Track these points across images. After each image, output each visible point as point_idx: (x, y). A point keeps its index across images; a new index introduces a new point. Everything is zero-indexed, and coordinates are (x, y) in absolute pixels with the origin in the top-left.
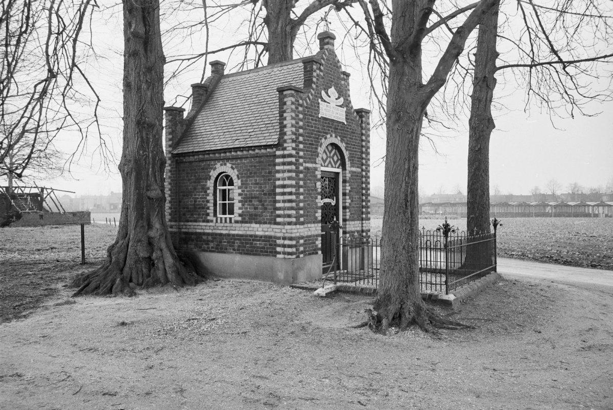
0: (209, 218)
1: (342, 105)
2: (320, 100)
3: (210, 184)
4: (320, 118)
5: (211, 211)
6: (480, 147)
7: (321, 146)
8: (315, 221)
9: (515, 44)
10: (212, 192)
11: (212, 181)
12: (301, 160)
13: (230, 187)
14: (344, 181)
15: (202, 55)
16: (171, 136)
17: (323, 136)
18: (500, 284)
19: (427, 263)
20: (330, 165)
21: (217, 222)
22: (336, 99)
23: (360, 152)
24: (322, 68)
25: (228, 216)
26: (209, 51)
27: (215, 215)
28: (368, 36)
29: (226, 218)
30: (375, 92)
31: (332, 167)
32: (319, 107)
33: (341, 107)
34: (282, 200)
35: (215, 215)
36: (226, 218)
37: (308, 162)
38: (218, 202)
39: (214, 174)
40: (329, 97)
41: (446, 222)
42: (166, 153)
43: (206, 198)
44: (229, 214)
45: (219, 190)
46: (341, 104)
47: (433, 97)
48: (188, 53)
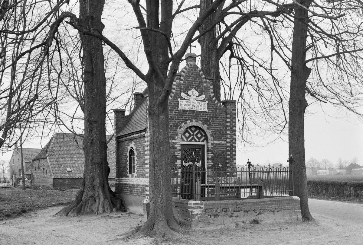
1: (204, 99)
2: (179, 100)
4: (180, 111)
7: (180, 129)
8: (177, 177)
12: (229, 145)
14: (208, 150)
16: (234, 128)
17: (183, 122)
18: (11, 122)
19: (270, 190)
20: (193, 140)
22: (197, 97)
23: (224, 130)
24: (182, 78)
31: (196, 141)
32: (178, 104)
33: (203, 101)
34: (202, 183)
37: (223, 144)
40: (190, 96)
41: (249, 161)
42: (26, 167)
46: (203, 99)
47: (84, 128)
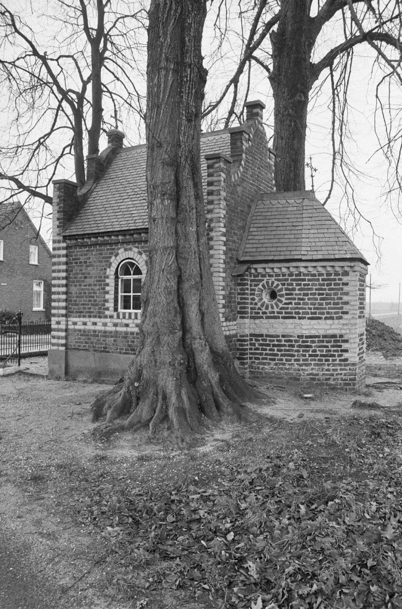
0: (107, 313)
3: (111, 272)
5: (111, 305)
6: (274, 155)
9: (246, 97)
10: (113, 296)
11: (113, 269)
13: (136, 277)
15: (116, 115)
21: (118, 317)
25: (132, 311)
26: (39, 185)
27: (116, 309)
28: (85, 121)
29: (130, 314)
30: (334, 145)
35: (116, 309)
36: (130, 314)
38: (120, 294)
39: (115, 262)
43: (105, 281)
44: (133, 309)
45: (122, 280)
48: (372, 119)
